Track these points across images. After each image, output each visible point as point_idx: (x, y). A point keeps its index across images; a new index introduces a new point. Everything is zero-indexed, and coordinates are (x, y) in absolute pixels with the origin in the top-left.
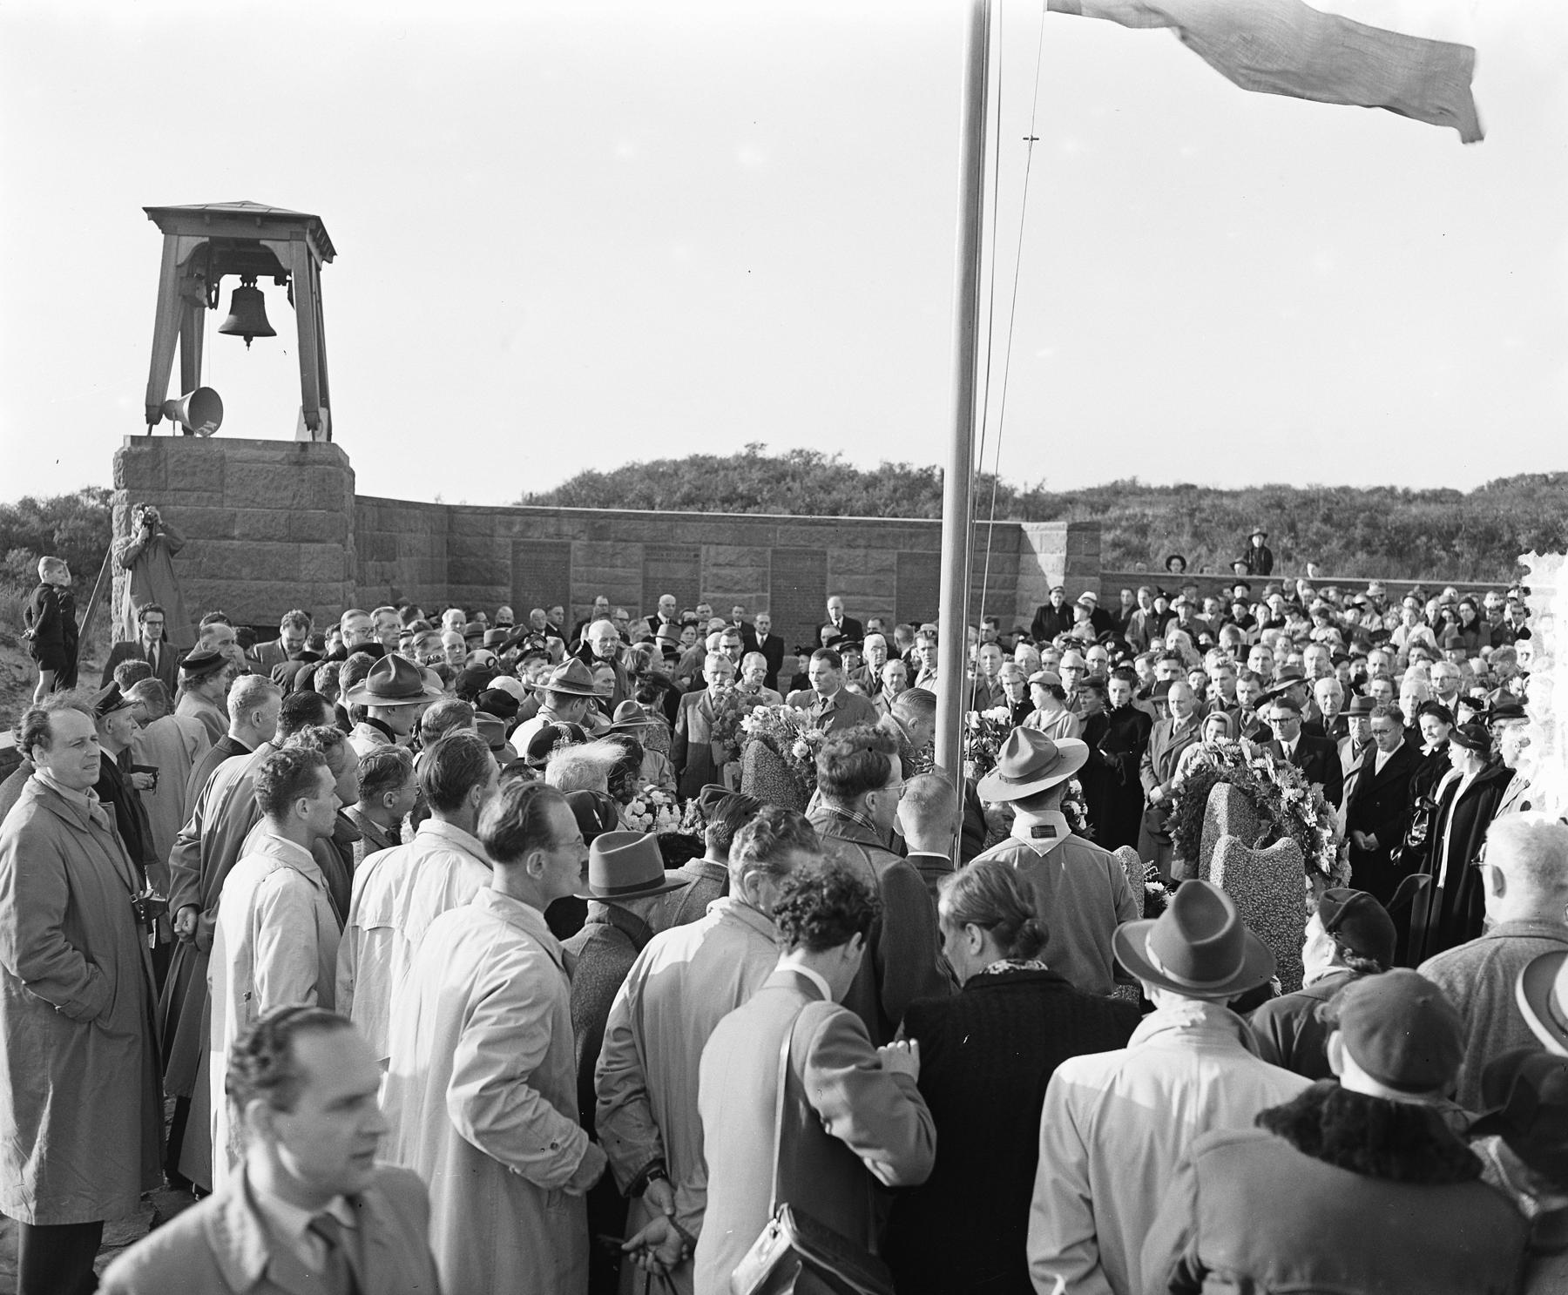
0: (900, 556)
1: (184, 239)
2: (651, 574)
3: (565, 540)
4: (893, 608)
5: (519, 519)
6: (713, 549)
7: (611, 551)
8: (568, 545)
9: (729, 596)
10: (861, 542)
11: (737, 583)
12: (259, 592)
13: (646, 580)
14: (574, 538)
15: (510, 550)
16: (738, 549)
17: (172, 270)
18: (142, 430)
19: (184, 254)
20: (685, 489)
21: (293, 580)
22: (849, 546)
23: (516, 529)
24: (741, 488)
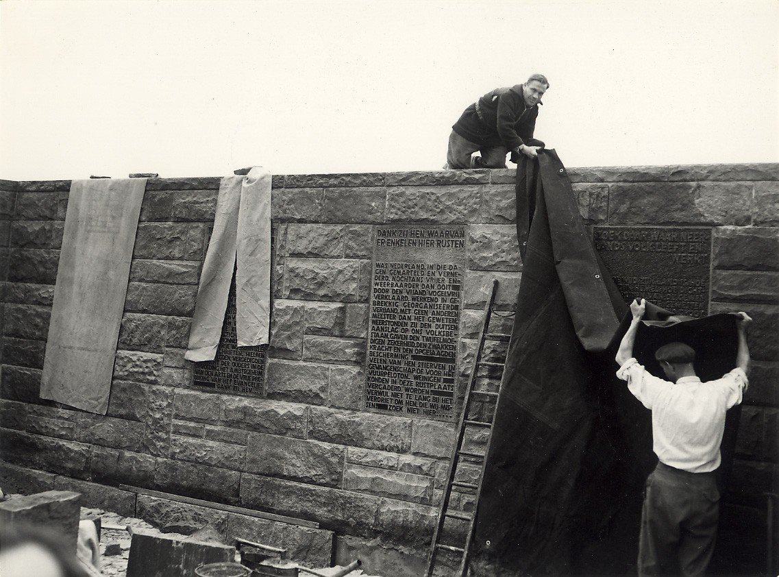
9: (310, 305)
11: (320, 285)
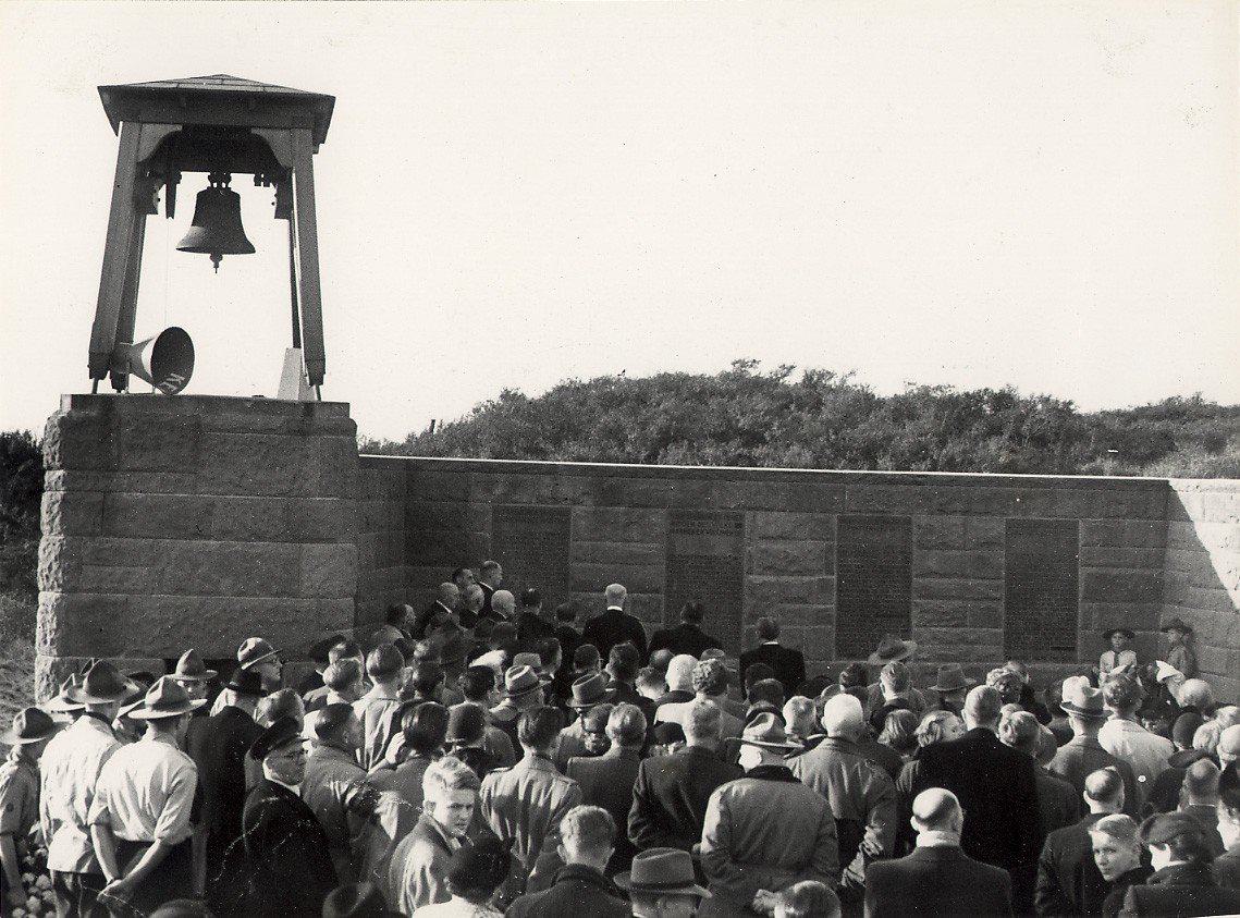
0: (1010, 525)
1: (148, 128)
2: (679, 550)
3: (564, 505)
4: (1002, 594)
5: (502, 477)
6: (761, 517)
7: (623, 519)
8: (566, 513)
9: (785, 579)
10: (959, 506)
12: (243, 612)
13: (671, 557)
14: (575, 502)
15: (489, 518)
16: (794, 517)
17: (131, 170)
18: (85, 387)
19: (147, 148)
20: (661, 421)
21: (294, 595)
22: (942, 512)
23: (498, 491)
24: (743, 423)
